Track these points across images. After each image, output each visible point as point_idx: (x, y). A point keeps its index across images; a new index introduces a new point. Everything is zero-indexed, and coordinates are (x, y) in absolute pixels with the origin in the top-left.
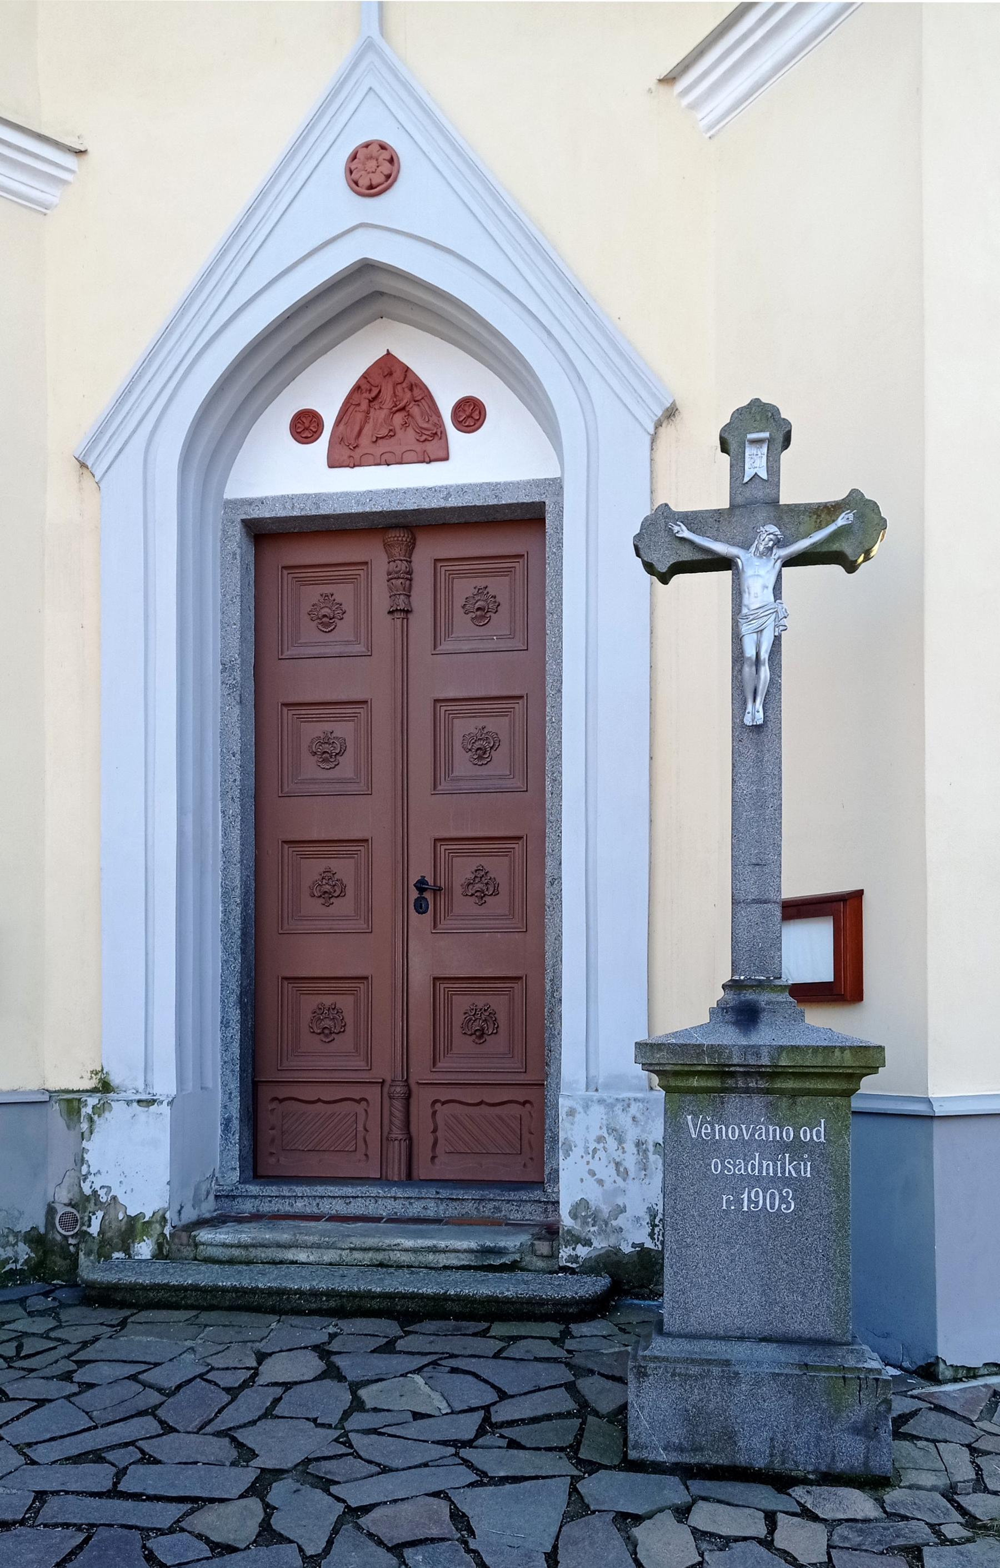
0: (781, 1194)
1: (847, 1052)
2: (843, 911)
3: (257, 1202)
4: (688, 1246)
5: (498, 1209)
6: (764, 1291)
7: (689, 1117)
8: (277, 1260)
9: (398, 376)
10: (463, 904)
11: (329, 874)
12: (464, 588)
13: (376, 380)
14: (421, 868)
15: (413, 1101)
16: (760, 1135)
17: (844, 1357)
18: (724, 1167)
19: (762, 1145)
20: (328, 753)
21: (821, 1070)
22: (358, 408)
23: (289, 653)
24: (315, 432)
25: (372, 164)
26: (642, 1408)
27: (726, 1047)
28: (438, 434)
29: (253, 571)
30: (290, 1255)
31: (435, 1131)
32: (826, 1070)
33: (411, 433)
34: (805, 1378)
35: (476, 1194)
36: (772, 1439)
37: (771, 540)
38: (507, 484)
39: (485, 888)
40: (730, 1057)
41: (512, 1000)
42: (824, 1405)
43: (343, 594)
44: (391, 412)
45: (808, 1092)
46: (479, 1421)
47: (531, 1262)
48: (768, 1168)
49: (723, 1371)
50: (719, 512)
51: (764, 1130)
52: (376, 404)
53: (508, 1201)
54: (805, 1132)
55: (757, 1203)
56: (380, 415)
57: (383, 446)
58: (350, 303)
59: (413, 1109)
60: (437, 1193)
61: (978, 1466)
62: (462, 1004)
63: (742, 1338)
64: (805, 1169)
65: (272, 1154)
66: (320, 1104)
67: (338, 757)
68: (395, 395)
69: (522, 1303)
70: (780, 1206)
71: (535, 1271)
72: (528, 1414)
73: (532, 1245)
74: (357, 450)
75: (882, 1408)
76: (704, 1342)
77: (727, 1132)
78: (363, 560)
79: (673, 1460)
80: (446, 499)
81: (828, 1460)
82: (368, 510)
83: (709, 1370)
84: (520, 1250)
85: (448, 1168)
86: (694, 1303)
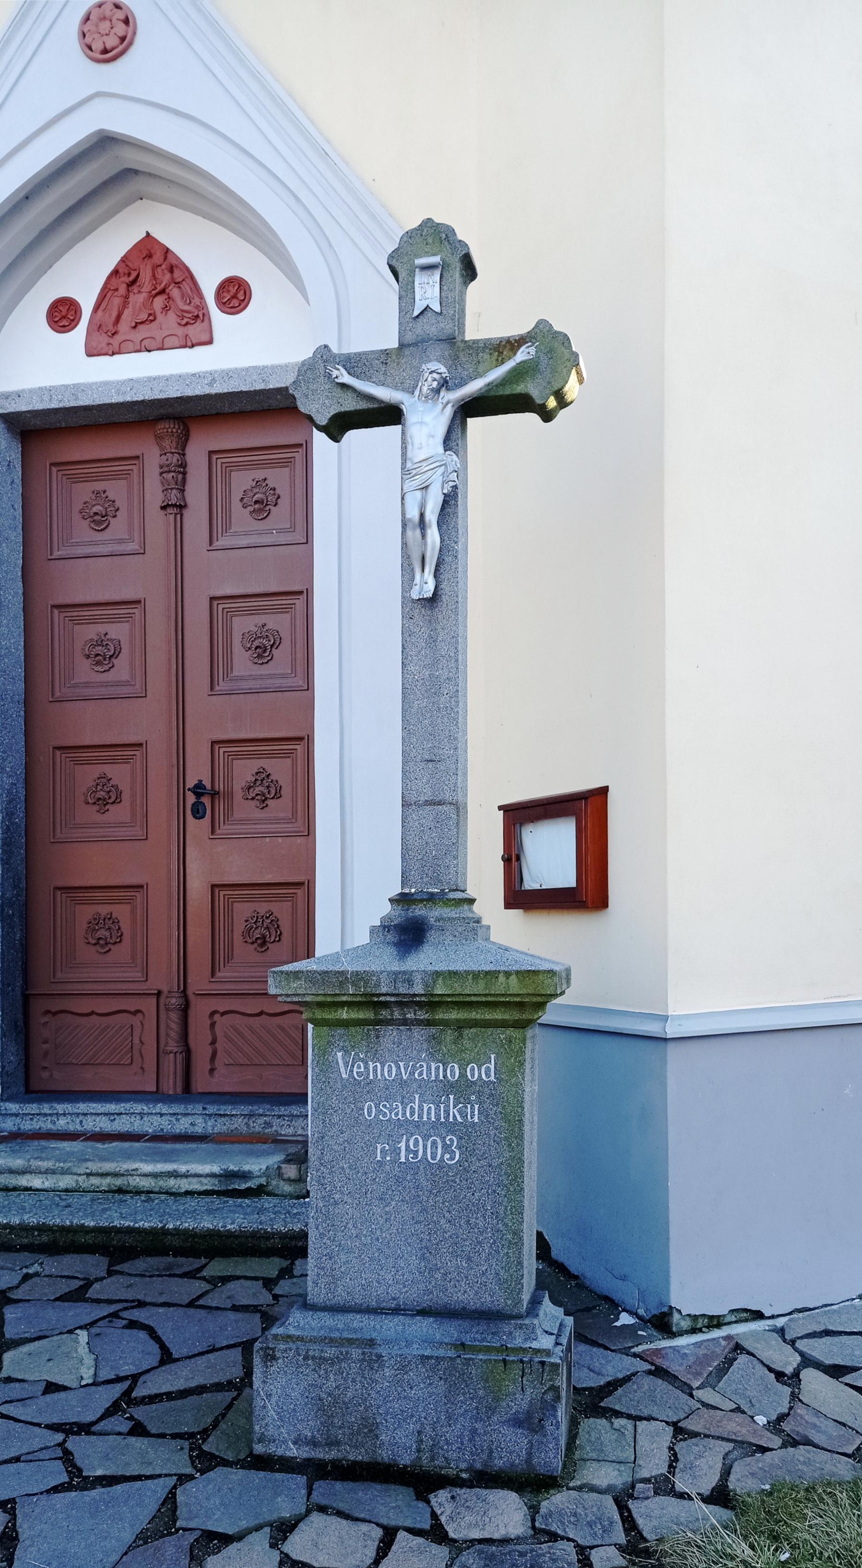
0: (444, 1141)
1: (513, 977)
2: (587, 810)
3: (18, 1120)
4: (336, 1203)
5: (268, 1124)
6: (423, 1255)
7: (339, 1054)
8: (11, 1186)
9: (158, 258)
10: (245, 809)
11: (104, 780)
12: (242, 481)
13: (135, 263)
14: (198, 771)
15: (192, 1013)
16: (421, 1074)
17: (511, 1333)
18: (379, 1111)
19: (422, 1085)
20: (104, 655)
21: (484, 999)
22: (116, 293)
23: (60, 553)
24: (73, 320)
25: (105, 26)
26: (269, 1396)
27: (373, 973)
28: (200, 316)
29: (19, 469)
30: (24, 1181)
31: (213, 1042)
32: (490, 999)
33: (172, 317)
34: (458, 1361)
35: (245, 1109)
36: (419, 1433)
37: (435, 380)
38: (274, 368)
39: (266, 791)
40: (377, 985)
41: (294, 908)
42: (481, 1392)
43: (116, 490)
44: (152, 294)
45: (474, 1024)
46: (117, 1395)
47: (277, 1186)
48: (429, 1112)
49: (363, 1353)
50: (386, 353)
51: (425, 1068)
52: (135, 289)
53: (279, 1117)
54: (473, 1069)
55: (416, 1153)
56: (138, 299)
57: (144, 331)
58: (97, 182)
59: (191, 1020)
60: (204, 1109)
61: (675, 1455)
62: (243, 911)
63: (396, 1311)
64: (473, 1112)
65: (45, 1068)
66: (94, 1016)
67: (113, 660)
68: (154, 276)
69: (247, 1237)
70: (442, 1156)
71: (282, 1196)
72: (180, 1384)
73: (279, 1168)
74: (115, 337)
75: (549, 1397)
76: (350, 1316)
77: (382, 1070)
78: (134, 454)
79: (305, 1455)
80: (210, 384)
81: (484, 1456)
82: (129, 399)
83: (347, 1353)
84: (267, 1173)
85: (224, 1081)
86: (343, 1269)
